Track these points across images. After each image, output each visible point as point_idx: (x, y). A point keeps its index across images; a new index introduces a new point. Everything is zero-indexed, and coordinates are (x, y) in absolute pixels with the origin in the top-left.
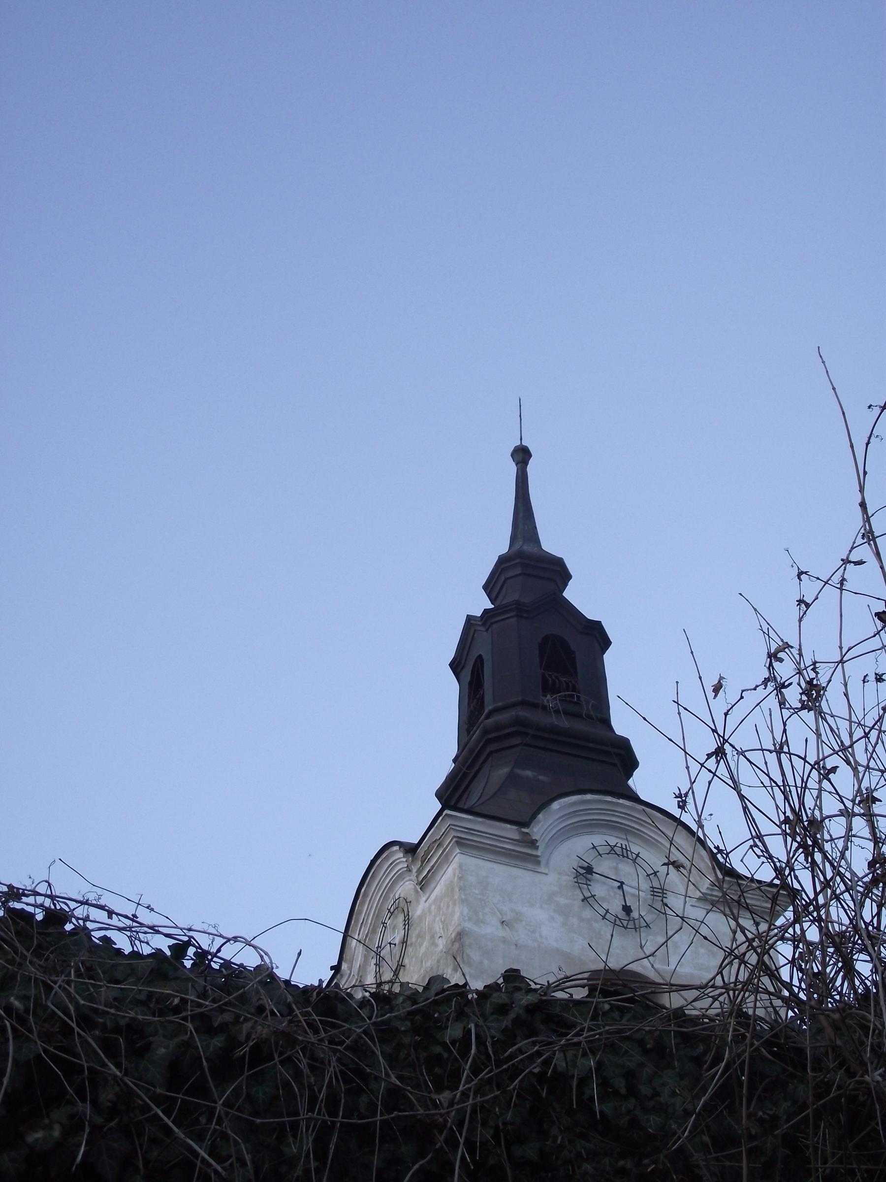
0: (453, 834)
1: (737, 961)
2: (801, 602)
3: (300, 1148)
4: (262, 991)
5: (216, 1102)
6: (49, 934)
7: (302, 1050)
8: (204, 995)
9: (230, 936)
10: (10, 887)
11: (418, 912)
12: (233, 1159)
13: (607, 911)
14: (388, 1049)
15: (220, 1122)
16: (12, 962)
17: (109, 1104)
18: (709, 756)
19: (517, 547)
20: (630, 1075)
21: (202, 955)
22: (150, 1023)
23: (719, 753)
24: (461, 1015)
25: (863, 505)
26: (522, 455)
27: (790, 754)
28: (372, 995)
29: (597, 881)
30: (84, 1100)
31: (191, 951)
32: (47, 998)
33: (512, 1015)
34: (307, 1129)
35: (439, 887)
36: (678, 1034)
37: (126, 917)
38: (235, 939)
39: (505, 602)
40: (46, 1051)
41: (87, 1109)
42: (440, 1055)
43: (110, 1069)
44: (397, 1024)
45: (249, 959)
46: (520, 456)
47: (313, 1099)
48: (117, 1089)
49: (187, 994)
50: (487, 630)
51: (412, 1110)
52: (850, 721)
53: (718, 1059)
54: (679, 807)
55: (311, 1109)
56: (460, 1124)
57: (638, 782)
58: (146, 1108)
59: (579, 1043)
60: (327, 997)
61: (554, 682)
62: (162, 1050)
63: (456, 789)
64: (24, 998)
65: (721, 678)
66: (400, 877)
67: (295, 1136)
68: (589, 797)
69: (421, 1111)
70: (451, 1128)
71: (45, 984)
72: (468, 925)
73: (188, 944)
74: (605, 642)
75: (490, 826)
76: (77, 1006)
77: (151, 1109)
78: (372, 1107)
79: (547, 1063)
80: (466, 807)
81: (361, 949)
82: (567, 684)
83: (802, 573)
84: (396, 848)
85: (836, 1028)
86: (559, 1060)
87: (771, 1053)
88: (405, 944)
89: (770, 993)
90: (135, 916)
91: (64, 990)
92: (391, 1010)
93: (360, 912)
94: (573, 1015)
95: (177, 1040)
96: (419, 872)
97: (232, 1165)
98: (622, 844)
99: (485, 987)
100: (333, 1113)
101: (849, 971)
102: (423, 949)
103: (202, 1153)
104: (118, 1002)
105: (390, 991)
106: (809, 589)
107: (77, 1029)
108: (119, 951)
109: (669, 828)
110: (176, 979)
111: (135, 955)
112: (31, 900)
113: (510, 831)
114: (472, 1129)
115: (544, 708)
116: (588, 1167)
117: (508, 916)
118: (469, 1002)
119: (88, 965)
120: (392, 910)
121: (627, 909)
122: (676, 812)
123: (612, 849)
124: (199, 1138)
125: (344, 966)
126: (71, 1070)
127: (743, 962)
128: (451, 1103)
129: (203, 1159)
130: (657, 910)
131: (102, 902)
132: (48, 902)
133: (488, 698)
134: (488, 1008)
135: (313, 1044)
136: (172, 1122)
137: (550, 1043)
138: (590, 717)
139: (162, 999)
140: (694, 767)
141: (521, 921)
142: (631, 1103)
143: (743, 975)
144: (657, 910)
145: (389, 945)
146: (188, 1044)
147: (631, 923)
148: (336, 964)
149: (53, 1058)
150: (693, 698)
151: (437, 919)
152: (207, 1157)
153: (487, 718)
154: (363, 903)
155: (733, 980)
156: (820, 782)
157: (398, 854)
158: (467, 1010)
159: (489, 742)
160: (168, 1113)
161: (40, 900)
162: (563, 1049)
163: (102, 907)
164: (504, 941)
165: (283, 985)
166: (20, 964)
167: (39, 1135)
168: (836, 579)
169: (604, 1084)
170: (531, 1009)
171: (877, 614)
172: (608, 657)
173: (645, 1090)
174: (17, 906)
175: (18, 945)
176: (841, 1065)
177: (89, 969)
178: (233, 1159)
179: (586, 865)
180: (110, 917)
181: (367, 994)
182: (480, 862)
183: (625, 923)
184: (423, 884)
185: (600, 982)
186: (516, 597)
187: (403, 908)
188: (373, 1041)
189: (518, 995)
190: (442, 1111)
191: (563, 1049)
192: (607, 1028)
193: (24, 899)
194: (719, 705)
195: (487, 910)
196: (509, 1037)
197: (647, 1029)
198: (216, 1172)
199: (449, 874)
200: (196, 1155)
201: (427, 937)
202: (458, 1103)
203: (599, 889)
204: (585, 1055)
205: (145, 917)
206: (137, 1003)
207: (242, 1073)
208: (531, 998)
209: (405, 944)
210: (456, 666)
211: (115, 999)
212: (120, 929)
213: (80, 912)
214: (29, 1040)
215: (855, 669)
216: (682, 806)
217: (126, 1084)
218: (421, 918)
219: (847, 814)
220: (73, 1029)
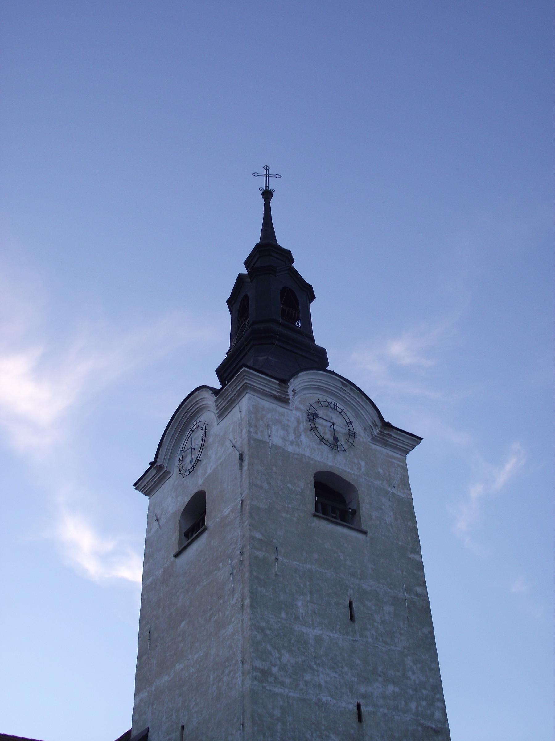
26: (267, 195)
50: (251, 282)
74: (312, 297)
88: (202, 448)
98: (334, 403)
120: (193, 429)
123: (329, 404)
130: (351, 443)
144: (351, 443)
145: (191, 449)
148: (153, 461)
172: (313, 305)
209: (202, 448)
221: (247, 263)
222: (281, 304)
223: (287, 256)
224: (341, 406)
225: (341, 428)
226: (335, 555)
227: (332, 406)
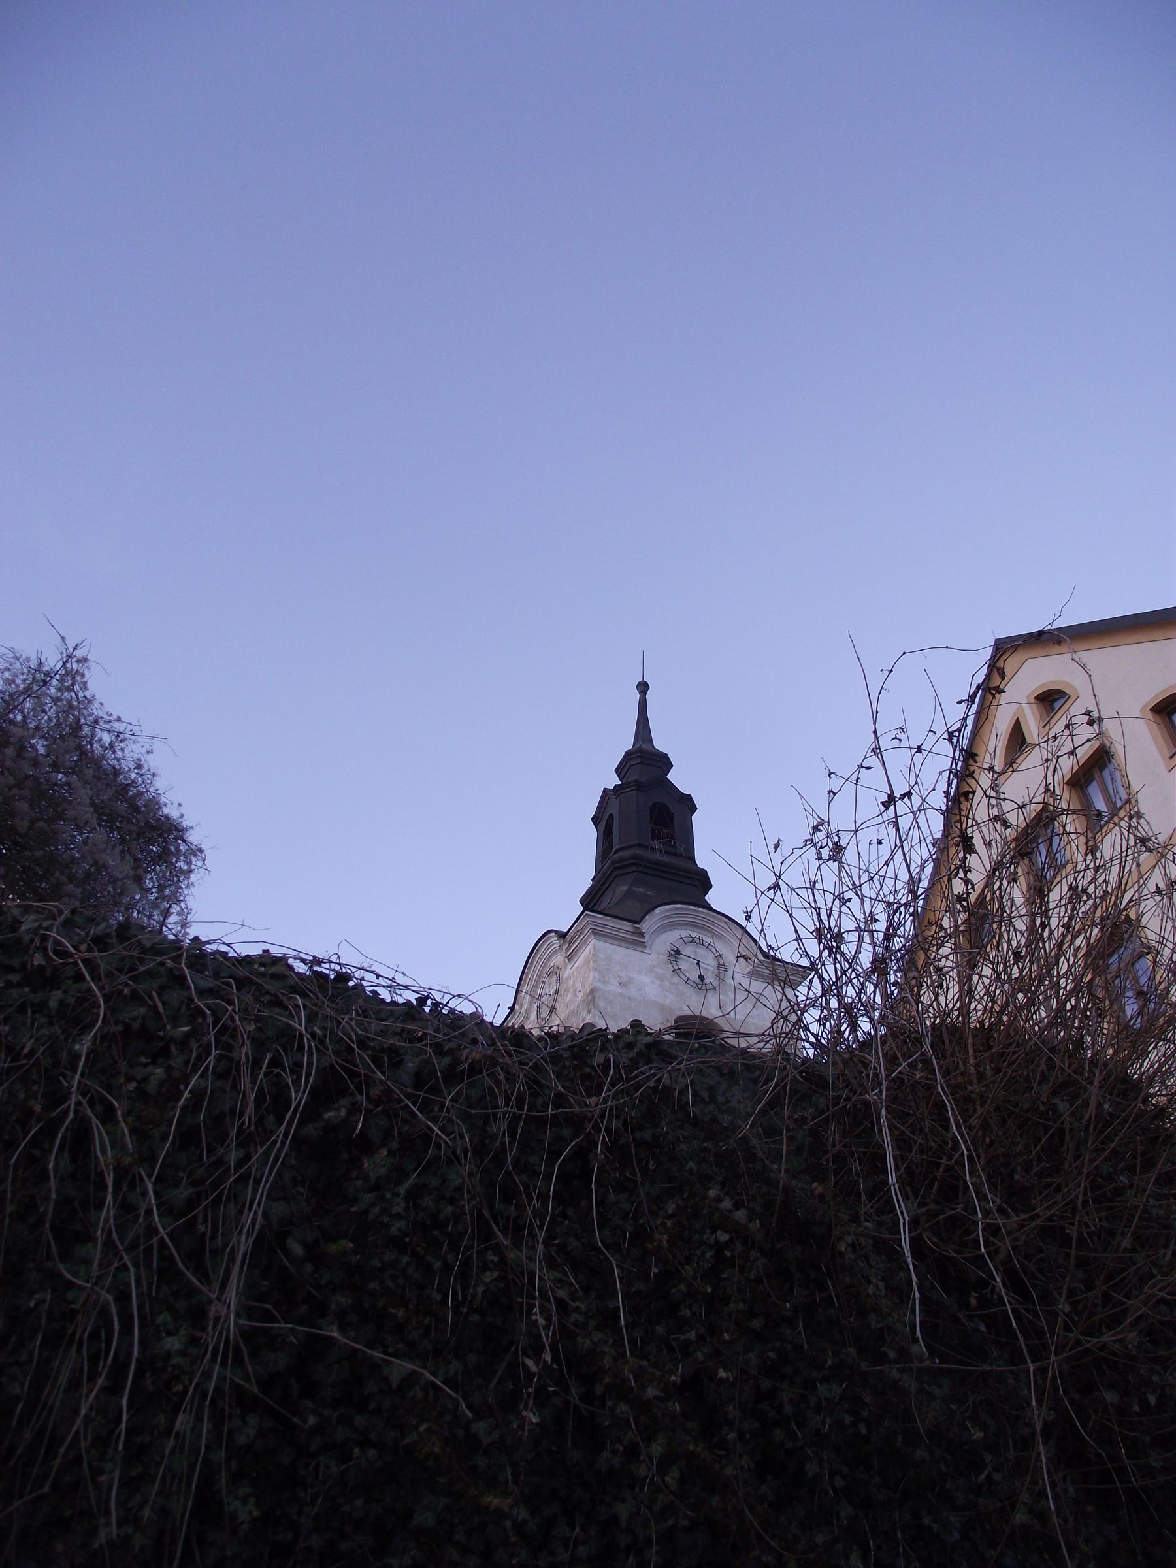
0: (590, 927)
1: (782, 1019)
2: (830, 791)
3: (499, 1128)
4: (476, 1030)
5: (445, 1098)
6: (338, 988)
7: (502, 1068)
8: (437, 1030)
9: (456, 994)
10: (314, 957)
11: (566, 975)
12: (456, 1134)
13: (689, 978)
14: (556, 1069)
15: (448, 1111)
16: (315, 1005)
17: (377, 1097)
18: (769, 889)
19: (638, 745)
20: (711, 1089)
21: (436, 1005)
22: (403, 1047)
23: (776, 887)
24: (604, 1048)
25: (875, 732)
26: (643, 687)
27: (824, 891)
28: (545, 1033)
29: (683, 959)
30: (361, 1094)
31: (429, 1002)
32: (338, 1028)
33: (636, 1050)
34: (504, 1118)
35: (580, 960)
36: (743, 1064)
37: (388, 979)
38: (459, 996)
39: (629, 780)
40: (337, 1062)
41: (362, 1099)
42: (590, 1074)
43: (377, 1075)
44: (563, 1052)
45: (467, 1008)
46: (642, 688)
47: (508, 1100)
48: (382, 1088)
49: (427, 1029)
51: (571, 1108)
52: (860, 869)
53: (769, 1080)
54: (746, 919)
55: (507, 1105)
56: (602, 1117)
57: (710, 898)
58: (400, 1101)
59: (680, 1069)
60: (517, 1034)
61: (659, 832)
62: (411, 1065)
63: (593, 898)
64: (324, 1028)
65: (779, 840)
66: (555, 952)
67: (495, 1121)
68: (679, 906)
69: (577, 1109)
70: (597, 1120)
71: (337, 1020)
72: (598, 985)
73: (428, 997)
75: (614, 922)
76: (357, 1034)
77: (403, 1101)
78: (546, 1105)
79: (659, 1081)
80: (599, 910)
81: (528, 997)
82: (668, 835)
83: (832, 773)
84: (553, 934)
85: (845, 1062)
86: (666, 1080)
87: (802, 1077)
89: (804, 1040)
90: (393, 978)
91: (348, 1024)
92: (558, 1044)
93: (528, 974)
94: (676, 1051)
95: (421, 1058)
96: (567, 949)
97: (455, 1137)
99: (618, 1031)
100: (521, 1108)
101: (854, 1026)
102: (568, 998)
103: (437, 1130)
104: (383, 1033)
105: (557, 1032)
106: (836, 784)
107: (356, 1049)
108: (383, 1000)
109: (739, 933)
110: (420, 1019)
111: (394, 1003)
112: (327, 965)
113: (627, 926)
114: (610, 1119)
115: (652, 849)
116: (684, 1146)
117: (624, 980)
118: (609, 1040)
119: (363, 1008)
121: (701, 978)
122: (743, 923)
123: (1063, 834)
124: (434, 1120)
125: (517, 1007)
126: (353, 1075)
127: (786, 1018)
128: (597, 1105)
129: (437, 1134)
131: (372, 969)
132: (338, 968)
133: (616, 841)
134: (621, 1045)
135: (508, 1064)
136: (417, 1109)
137: (660, 1069)
138: (681, 855)
139: (410, 1032)
140: (759, 894)
141: (632, 983)
142: (712, 1107)
143: (786, 1029)
146: (427, 1062)
147: (704, 986)
149: (341, 1066)
150: (761, 853)
151: (578, 979)
152: (440, 1133)
153: (615, 853)
154: (530, 969)
155: (779, 1031)
156: (840, 907)
157: (554, 938)
158: (608, 1045)
159: (615, 869)
160: (414, 1104)
161: (333, 966)
162: (670, 1072)
163: (372, 972)
164: (621, 995)
165: (490, 1027)
166: (320, 1007)
167: (332, 1114)
168: (854, 777)
169: (696, 1094)
170: (649, 1046)
171: (882, 803)
173: (721, 1099)
174: (319, 969)
175: (319, 995)
176: (847, 1087)
177: (364, 1011)
178: (456, 1134)
179: (676, 949)
180: (377, 978)
181: (543, 1033)
182: (607, 945)
183: (700, 986)
184: (570, 958)
185: (695, 1030)
186: (636, 778)
187: (556, 972)
188: (547, 1063)
189: (640, 1037)
190: (591, 1109)
191: (670, 1072)
192: (699, 1060)
193: (323, 965)
194: (777, 857)
195: (610, 976)
196: (633, 1065)
197: (724, 1061)
198: (445, 1142)
199: (586, 952)
200: (433, 1131)
201: (571, 991)
202: (601, 1104)
203: (683, 964)
204: (684, 1075)
205: (400, 979)
206: (395, 1034)
207: (463, 1080)
208: (649, 1039)
210: (596, 820)
211: (381, 1031)
212: (384, 987)
213: (358, 974)
214: (325, 1054)
215: (864, 836)
216: (748, 918)
217: (387, 1085)
218: (567, 978)
219: (858, 929)
220: (354, 1050)
221: (619, 771)
222: (651, 820)
223: (664, 762)
224: (707, 940)
225: (709, 961)
226: (855, 1178)
227: (697, 941)
